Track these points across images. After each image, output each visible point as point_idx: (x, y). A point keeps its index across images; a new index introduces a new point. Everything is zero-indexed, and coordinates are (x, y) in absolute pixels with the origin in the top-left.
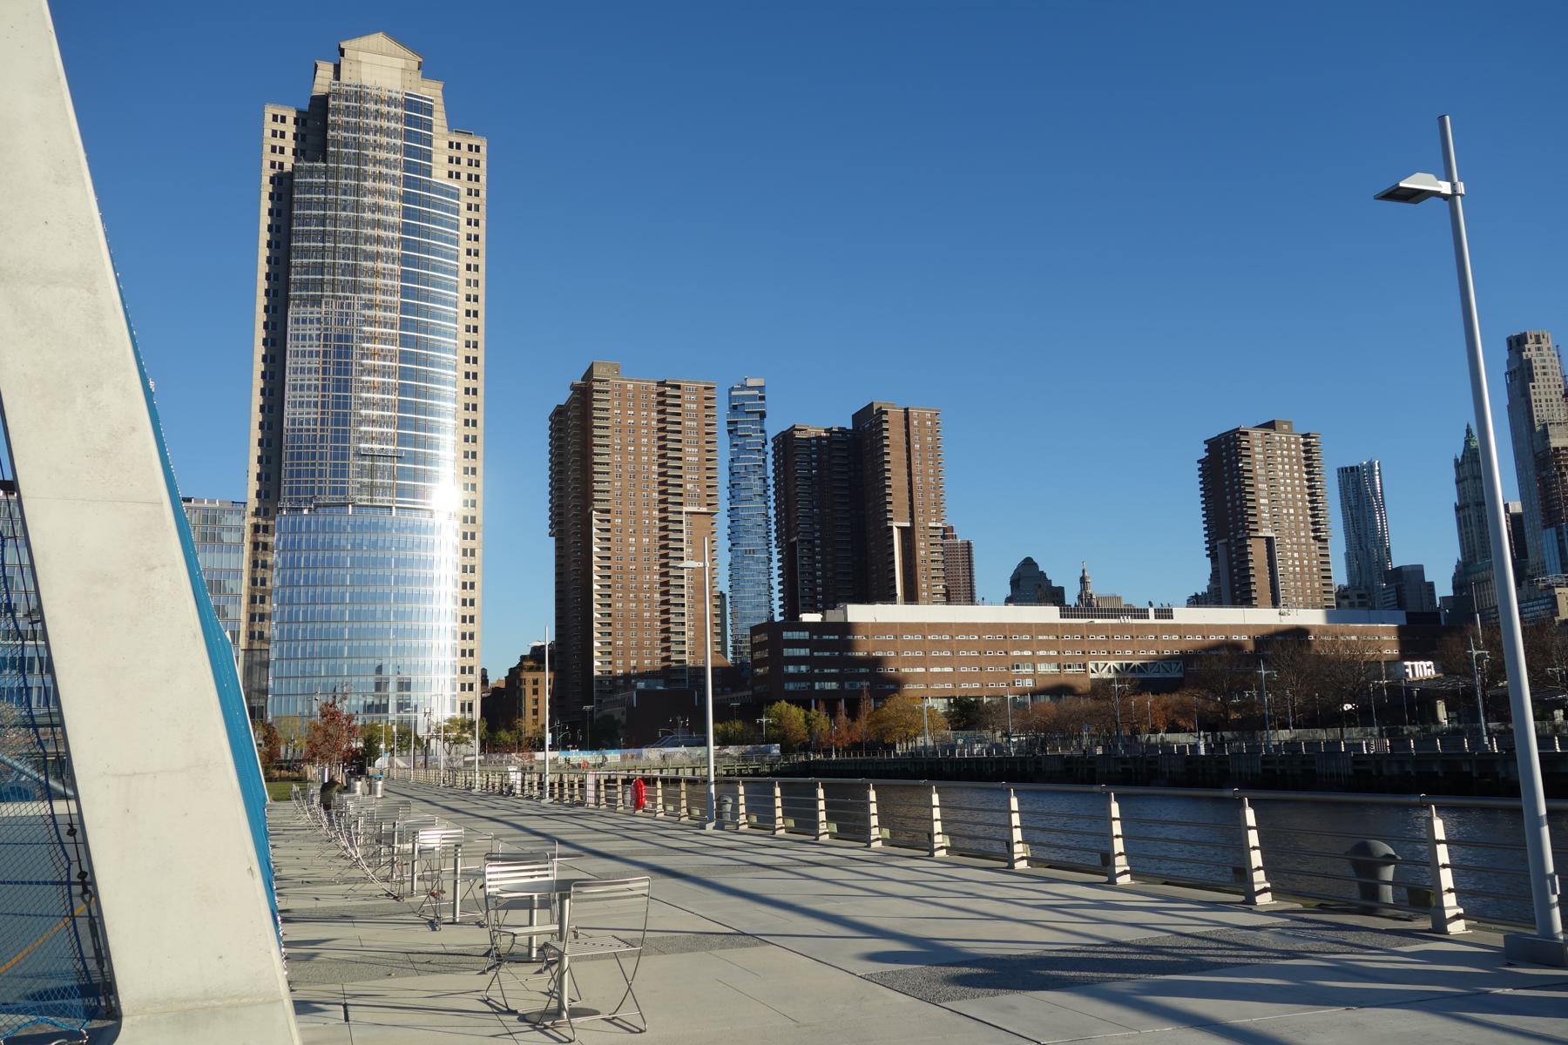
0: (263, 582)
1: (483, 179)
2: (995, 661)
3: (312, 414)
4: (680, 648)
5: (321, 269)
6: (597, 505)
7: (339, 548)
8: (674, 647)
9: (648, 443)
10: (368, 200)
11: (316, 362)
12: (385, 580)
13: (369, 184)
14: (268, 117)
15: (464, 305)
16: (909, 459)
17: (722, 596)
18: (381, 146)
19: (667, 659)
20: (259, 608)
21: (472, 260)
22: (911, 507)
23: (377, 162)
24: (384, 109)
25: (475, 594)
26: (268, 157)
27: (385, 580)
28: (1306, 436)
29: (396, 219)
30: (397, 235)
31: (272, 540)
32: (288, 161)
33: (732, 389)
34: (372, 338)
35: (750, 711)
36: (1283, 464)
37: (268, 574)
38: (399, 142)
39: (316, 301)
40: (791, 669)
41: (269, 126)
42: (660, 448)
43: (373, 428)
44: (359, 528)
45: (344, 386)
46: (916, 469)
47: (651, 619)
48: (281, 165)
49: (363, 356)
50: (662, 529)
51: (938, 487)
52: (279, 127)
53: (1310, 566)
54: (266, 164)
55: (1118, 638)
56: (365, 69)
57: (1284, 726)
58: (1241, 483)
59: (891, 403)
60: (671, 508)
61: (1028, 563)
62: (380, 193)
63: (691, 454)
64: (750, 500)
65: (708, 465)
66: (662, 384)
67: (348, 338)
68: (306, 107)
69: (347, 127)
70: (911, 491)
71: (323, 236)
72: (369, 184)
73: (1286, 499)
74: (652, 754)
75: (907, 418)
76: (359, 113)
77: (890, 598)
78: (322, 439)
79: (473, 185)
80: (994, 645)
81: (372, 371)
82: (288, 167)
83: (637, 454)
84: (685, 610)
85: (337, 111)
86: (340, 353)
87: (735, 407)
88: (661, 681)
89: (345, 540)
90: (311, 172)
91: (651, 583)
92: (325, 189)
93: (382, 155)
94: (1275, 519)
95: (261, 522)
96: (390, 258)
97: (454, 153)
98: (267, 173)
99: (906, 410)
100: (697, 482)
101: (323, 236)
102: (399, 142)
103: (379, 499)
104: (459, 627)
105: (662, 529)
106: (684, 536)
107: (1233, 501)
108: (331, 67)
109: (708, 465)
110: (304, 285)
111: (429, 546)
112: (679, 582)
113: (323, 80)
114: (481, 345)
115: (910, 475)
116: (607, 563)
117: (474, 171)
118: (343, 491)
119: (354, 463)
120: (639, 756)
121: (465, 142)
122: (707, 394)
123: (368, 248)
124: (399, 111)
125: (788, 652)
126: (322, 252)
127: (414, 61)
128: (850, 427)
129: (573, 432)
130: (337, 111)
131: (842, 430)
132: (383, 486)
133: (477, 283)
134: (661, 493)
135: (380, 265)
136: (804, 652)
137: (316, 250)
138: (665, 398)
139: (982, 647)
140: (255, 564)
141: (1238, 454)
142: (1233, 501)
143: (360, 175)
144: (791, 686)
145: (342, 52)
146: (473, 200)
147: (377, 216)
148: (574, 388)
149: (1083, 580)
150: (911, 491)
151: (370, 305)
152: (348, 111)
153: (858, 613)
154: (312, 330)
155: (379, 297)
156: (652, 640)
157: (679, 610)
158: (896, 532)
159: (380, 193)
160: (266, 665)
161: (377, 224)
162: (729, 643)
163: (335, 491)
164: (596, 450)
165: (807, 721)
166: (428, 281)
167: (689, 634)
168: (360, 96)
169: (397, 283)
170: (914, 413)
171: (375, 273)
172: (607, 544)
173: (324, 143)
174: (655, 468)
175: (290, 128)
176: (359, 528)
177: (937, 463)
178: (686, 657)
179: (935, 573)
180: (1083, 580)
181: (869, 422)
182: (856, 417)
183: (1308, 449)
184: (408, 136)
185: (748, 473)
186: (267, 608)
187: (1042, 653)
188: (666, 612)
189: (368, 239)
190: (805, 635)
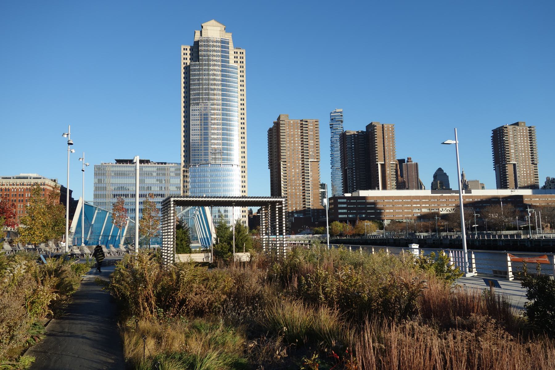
0: (186, 187)
1: (244, 62)
3: (198, 137)
4: (309, 204)
5: (199, 94)
6: (282, 160)
9: (298, 140)
11: (198, 122)
12: (220, 185)
13: (211, 67)
14: (182, 49)
15: (240, 83)
16: (384, 141)
18: (214, 56)
21: (242, 88)
22: (384, 157)
23: (214, 60)
24: (215, 44)
25: (245, 179)
26: (183, 61)
27: (220, 185)
28: (530, 127)
29: (219, 78)
30: (220, 82)
31: (188, 174)
32: (188, 62)
33: (331, 113)
34: (214, 114)
36: (521, 138)
38: (219, 54)
39: (198, 104)
41: (183, 52)
43: (215, 143)
45: (206, 129)
47: (300, 195)
48: (186, 63)
49: (211, 120)
50: (303, 167)
51: (393, 150)
52: (185, 52)
53: (530, 174)
54: (182, 63)
55: (450, 200)
56: (209, 31)
58: (504, 145)
60: (305, 160)
61: (440, 170)
62: (215, 70)
66: (302, 121)
67: (207, 115)
68: (193, 45)
69: (205, 51)
70: (384, 152)
71: (199, 84)
72: (211, 67)
73: (521, 150)
75: (383, 128)
76: (208, 46)
78: (201, 145)
79: (242, 65)
81: (214, 124)
82: (188, 64)
83: (294, 143)
84: (310, 192)
85: (202, 46)
86: (205, 119)
88: (302, 214)
89: (208, 174)
90: (195, 65)
91: (299, 184)
92: (199, 70)
93: (215, 58)
94: (517, 157)
95: (185, 169)
97: (236, 55)
98: (183, 66)
100: (313, 152)
101: (199, 84)
103: (218, 162)
105: (303, 167)
106: (309, 169)
107: (501, 151)
108: (199, 32)
110: (194, 99)
112: (308, 183)
113: (197, 37)
114: (245, 86)
115: (384, 146)
116: (285, 178)
117: (242, 60)
118: (207, 160)
120: (290, 237)
121: (239, 51)
122: (316, 123)
123: (212, 87)
124: (219, 44)
126: (199, 89)
127: (223, 27)
129: (275, 136)
130: (202, 46)
131: (362, 132)
132: (218, 158)
133: (243, 95)
134: (302, 155)
135: (215, 92)
136: (345, 206)
138: (303, 125)
141: (503, 135)
142: (501, 151)
143: (209, 65)
144: (340, 216)
145: (202, 27)
146: (242, 69)
147: (214, 77)
148: (274, 123)
150: (384, 152)
151: (213, 104)
152: (205, 46)
153: (363, 193)
154: (197, 113)
155: (215, 102)
157: (308, 192)
158: (379, 166)
159: (215, 70)
161: (214, 80)
166: (229, 72)
168: (208, 41)
169: (221, 97)
170: (385, 126)
171: (214, 95)
172: (285, 172)
173: (198, 56)
174: (300, 147)
175: (188, 52)
177: (393, 142)
178: (311, 207)
179: (392, 178)
181: (371, 127)
183: (530, 132)
187: (423, 205)
188: (304, 193)
189: (212, 84)
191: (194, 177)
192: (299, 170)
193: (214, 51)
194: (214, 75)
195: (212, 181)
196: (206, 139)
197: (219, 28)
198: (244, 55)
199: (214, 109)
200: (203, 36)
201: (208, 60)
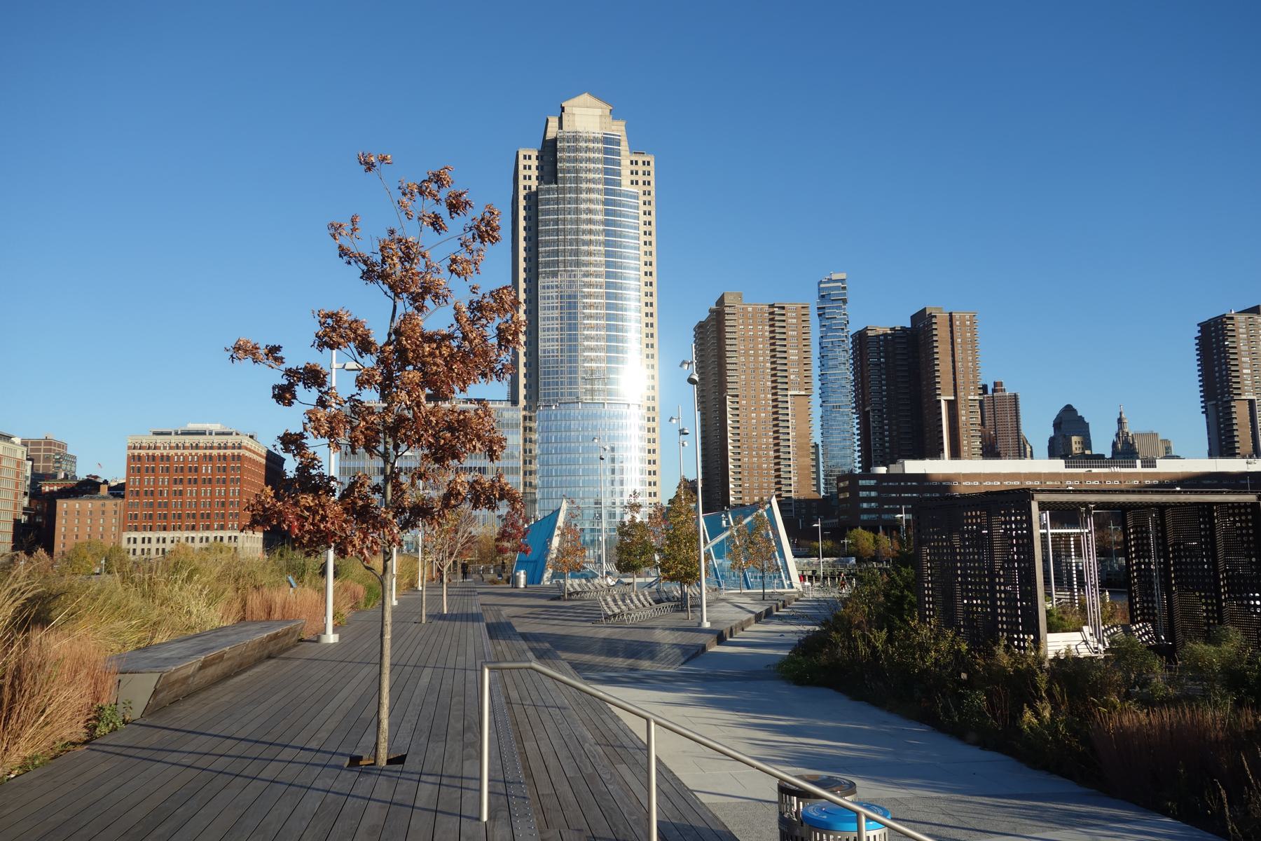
1: (653, 183)
3: (555, 346)
5: (557, 253)
6: (730, 392)
8: (784, 488)
9: (764, 348)
10: (583, 206)
11: (556, 313)
13: (584, 196)
17: (816, 446)
18: (590, 170)
20: (528, 467)
24: (591, 145)
25: (655, 320)
29: (600, 217)
30: (601, 228)
31: (534, 425)
32: (534, 184)
33: (821, 282)
34: (589, 296)
35: (837, 533)
37: (533, 446)
38: (600, 166)
39: (555, 274)
40: (865, 505)
42: (772, 350)
43: (591, 357)
45: (573, 327)
46: (958, 357)
49: (584, 307)
51: (975, 370)
59: (938, 306)
60: (780, 392)
61: (1069, 409)
62: (590, 201)
63: (793, 354)
64: (835, 367)
65: (805, 362)
66: (772, 306)
67: (575, 297)
69: (569, 160)
71: (557, 232)
72: (584, 196)
75: (951, 320)
76: (576, 150)
77: (936, 453)
79: (647, 188)
81: (590, 317)
82: (534, 188)
83: (756, 356)
85: (563, 150)
86: (570, 305)
90: (548, 191)
92: (557, 201)
93: (591, 176)
95: (527, 413)
96: (598, 243)
97: (634, 168)
100: (798, 374)
101: (557, 232)
102: (600, 166)
106: (789, 412)
107: (1220, 371)
108: (557, 119)
109: (805, 362)
110: (547, 264)
113: (552, 131)
115: (954, 361)
117: (647, 178)
119: (581, 374)
121: (640, 159)
124: (600, 145)
125: (863, 494)
128: (909, 325)
129: (712, 338)
130: (563, 150)
131: (903, 329)
134: (773, 382)
135: (592, 248)
137: (554, 241)
138: (775, 315)
140: (525, 440)
142: (1220, 371)
143: (578, 191)
144: (864, 517)
147: (589, 216)
148: (711, 311)
149: (1120, 421)
151: (587, 275)
152: (569, 149)
156: (769, 483)
157: (787, 462)
158: (943, 405)
159: (590, 201)
160: (535, 501)
161: (590, 221)
162: (822, 476)
163: (570, 394)
164: (728, 354)
165: (876, 541)
167: (794, 479)
168: (576, 139)
169: (603, 259)
170: (956, 316)
171: (590, 254)
173: (555, 171)
174: (768, 365)
175: (534, 163)
177: (974, 351)
180: (1120, 421)
181: (923, 321)
182: (914, 318)
184: (606, 172)
185: (834, 346)
186: (533, 467)
188: (778, 464)
189: (584, 232)
190: (873, 482)
191: (547, 430)
192: (766, 415)
193: (589, 160)
194: (590, 211)
196: (572, 349)
197: (598, 112)
198: (652, 168)
199: (590, 285)
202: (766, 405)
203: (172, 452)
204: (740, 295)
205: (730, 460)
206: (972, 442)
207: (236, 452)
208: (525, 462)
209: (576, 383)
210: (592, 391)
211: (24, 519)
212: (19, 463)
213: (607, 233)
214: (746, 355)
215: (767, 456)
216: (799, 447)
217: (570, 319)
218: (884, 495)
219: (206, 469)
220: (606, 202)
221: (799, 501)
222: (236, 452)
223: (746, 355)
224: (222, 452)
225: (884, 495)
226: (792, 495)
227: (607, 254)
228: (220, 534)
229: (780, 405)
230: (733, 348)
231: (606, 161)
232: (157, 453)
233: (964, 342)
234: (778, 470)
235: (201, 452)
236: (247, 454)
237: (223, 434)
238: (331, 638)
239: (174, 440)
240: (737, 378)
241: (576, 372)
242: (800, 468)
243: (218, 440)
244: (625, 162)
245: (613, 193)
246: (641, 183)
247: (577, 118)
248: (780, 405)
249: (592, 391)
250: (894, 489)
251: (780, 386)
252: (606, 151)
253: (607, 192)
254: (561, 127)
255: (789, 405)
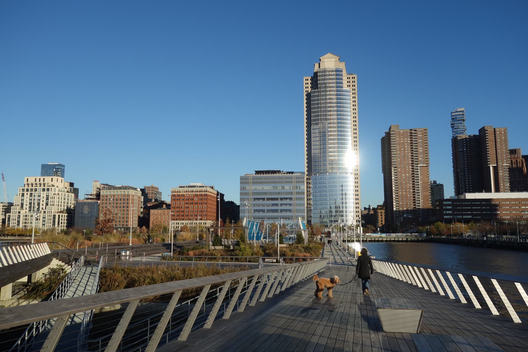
2: (515, 210)
3: (318, 151)
5: (318, 116)
6: (393, 166)
7: (325, 183)
9: (408, 147)
11: (318, 139)
13: (328, 93)
16: (496, 144)
19: (415, 208)
23: (330, 87)
24: (331, 73)
25: (357, 139)
26: (305, 90)
29: (334, 101)
31: (310, 181)
32: (309, 90)
33: (452, 113)
34: (331, 131)
39: (317, 124)
41: (305, 82)
42: (412, 148)
43: (332, 154)
44: (330, 178)
45: (325, 144)
47: (410, 197)
49: (329, 136)
54: (305, 91)
57: (506, 234)
59: (489, 124)
62: (331, 95)
63: (420, 150)
66: (411, 130)
67: (325, 132)
70: (496, 155)
71: (318, 108)
72: (328, 93)
74: (393, 235)
75: (495, 131)
77: (489, 190)
79: (354, 88)
80: (515, 205)
81: (331, 140)
82: (309, 91)
83: (404, 151)
85: (320, 76)
86: (323, 135)
87: (453, 119)
90: (314, 92)
92: (318, 96)
93: (331, 85)
95: (308, 177)
96: (334, 111)
98: (305, 93)
99: (494, 129)
100: (423, 158)
101: (318, 108)
104: (354, 201)
106: (419, 173)
108: (318, 64)
110: (315, 120)
111: (347, 182)
113: (316, 68)
115: (496, 149)
117: (354, 84)
118: (326, 169)
119: (328, 162)
121: (351, 76)
123: (329, 109)
129: (386, 142)
130: (320, 76)
131: (475, 136)
135: (332, 113)
139: (511, 206)
140: (307, 187)
150: (496, 155)
151: (329, 124)
154: (317, 131)
157: (418, 194)
158: (491, 168)
159: (331, 95)
160: (311, 210)
161: (331, 103)
168: (325, 71)
171: (331, 115)
173: (317, 84)
174: (410, 154)
175: (309, 82)
176: (330, 178)
181: (483, 131)
184: (337, 83)
189: (328, 107)
191: (315, 183)
193: (330, 79)
194: (330, 99)
195: (330, 191)
196: (325, 152)
197: (334, 60)
198: (356, 80)
199: (331, 127)
200: (321, 67)
201: (326, 87)
202: (409, 171)
203: (185, 193)
204: (398, 126)
205: (394, 193)
206: (505, 183)
207: (205, 193)
208: (307, 196)
209: (326, 165)
210: (332, 168)
211: (141, 216)
212: (139, 197)
213: (338, 107)
214: (400, 150)
215: (410, 192)
216: (424, 188)
217: (323, 141)
218: (454, 208)
219: (196, 199)
220: (337, 95)
221: (423, 210)
222: (205, 193)
223: (400, 150)
224: (201, 193)
225: (454, 208)
226: (421, 207)
227: (338, 115)
228: (201, 221)
229: (415, 170)
230: (395, 148)
231: (337, 79)
232: (180, 194)
233: (501, 141)
234: (414, 197)
235: (194, 193)
236: (209, 194)
237: (201, 187)
238: (131, 244)
239: (185, 189)
240: (396, 160)
241: (326, 161)
242: (424, 197)
243: (199, 189)
244: (345, 78)
245: (340, 91)
246: (351, 86)
247: (325, 63)
248: (415, 170)
249: (332, 168)
250: (459, 205)
251: (415, 163)
252: (337, 75)
253: (337, 91)
254: (319, 67)
255: (419, 170)
